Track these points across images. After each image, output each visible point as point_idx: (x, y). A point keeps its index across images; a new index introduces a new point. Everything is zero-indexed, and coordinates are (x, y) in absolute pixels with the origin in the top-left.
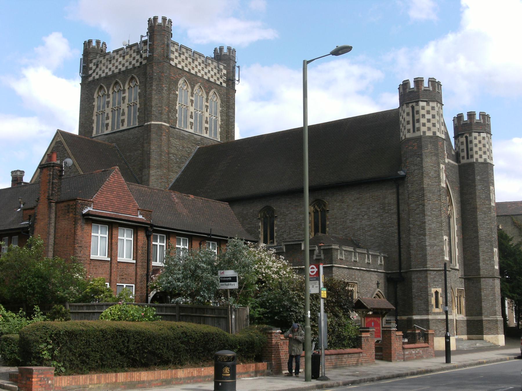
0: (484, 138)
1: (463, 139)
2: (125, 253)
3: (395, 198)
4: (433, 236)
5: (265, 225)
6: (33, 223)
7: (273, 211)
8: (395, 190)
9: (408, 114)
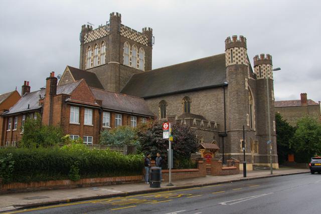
0: (268, 67)
1: (258, 68)
2: (88, 120)
5: (161, 109)
6: (43, 106)
8: (223, 91)
9: (229, 54)
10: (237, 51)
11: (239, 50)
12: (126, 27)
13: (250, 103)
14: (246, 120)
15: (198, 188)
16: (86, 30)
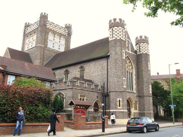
0: (145, 45)
3: (106, 64)
4: (119, 77)
7: (69, 72)
8: (106, 61)
10: (116, 29)
11: (118, 29)
12: (61, 27)
13: (131, 72)
14: (123, 83)
15: (167, 128)
16: (27, 26)
